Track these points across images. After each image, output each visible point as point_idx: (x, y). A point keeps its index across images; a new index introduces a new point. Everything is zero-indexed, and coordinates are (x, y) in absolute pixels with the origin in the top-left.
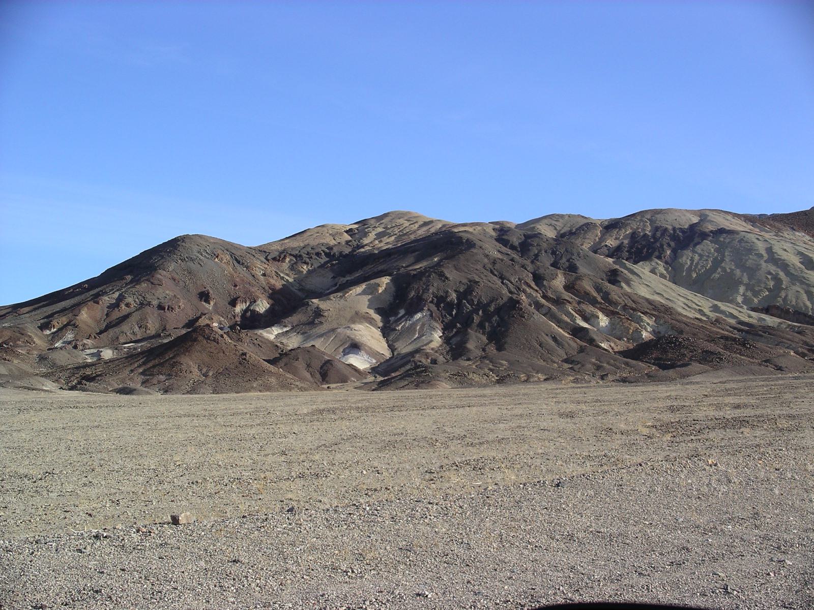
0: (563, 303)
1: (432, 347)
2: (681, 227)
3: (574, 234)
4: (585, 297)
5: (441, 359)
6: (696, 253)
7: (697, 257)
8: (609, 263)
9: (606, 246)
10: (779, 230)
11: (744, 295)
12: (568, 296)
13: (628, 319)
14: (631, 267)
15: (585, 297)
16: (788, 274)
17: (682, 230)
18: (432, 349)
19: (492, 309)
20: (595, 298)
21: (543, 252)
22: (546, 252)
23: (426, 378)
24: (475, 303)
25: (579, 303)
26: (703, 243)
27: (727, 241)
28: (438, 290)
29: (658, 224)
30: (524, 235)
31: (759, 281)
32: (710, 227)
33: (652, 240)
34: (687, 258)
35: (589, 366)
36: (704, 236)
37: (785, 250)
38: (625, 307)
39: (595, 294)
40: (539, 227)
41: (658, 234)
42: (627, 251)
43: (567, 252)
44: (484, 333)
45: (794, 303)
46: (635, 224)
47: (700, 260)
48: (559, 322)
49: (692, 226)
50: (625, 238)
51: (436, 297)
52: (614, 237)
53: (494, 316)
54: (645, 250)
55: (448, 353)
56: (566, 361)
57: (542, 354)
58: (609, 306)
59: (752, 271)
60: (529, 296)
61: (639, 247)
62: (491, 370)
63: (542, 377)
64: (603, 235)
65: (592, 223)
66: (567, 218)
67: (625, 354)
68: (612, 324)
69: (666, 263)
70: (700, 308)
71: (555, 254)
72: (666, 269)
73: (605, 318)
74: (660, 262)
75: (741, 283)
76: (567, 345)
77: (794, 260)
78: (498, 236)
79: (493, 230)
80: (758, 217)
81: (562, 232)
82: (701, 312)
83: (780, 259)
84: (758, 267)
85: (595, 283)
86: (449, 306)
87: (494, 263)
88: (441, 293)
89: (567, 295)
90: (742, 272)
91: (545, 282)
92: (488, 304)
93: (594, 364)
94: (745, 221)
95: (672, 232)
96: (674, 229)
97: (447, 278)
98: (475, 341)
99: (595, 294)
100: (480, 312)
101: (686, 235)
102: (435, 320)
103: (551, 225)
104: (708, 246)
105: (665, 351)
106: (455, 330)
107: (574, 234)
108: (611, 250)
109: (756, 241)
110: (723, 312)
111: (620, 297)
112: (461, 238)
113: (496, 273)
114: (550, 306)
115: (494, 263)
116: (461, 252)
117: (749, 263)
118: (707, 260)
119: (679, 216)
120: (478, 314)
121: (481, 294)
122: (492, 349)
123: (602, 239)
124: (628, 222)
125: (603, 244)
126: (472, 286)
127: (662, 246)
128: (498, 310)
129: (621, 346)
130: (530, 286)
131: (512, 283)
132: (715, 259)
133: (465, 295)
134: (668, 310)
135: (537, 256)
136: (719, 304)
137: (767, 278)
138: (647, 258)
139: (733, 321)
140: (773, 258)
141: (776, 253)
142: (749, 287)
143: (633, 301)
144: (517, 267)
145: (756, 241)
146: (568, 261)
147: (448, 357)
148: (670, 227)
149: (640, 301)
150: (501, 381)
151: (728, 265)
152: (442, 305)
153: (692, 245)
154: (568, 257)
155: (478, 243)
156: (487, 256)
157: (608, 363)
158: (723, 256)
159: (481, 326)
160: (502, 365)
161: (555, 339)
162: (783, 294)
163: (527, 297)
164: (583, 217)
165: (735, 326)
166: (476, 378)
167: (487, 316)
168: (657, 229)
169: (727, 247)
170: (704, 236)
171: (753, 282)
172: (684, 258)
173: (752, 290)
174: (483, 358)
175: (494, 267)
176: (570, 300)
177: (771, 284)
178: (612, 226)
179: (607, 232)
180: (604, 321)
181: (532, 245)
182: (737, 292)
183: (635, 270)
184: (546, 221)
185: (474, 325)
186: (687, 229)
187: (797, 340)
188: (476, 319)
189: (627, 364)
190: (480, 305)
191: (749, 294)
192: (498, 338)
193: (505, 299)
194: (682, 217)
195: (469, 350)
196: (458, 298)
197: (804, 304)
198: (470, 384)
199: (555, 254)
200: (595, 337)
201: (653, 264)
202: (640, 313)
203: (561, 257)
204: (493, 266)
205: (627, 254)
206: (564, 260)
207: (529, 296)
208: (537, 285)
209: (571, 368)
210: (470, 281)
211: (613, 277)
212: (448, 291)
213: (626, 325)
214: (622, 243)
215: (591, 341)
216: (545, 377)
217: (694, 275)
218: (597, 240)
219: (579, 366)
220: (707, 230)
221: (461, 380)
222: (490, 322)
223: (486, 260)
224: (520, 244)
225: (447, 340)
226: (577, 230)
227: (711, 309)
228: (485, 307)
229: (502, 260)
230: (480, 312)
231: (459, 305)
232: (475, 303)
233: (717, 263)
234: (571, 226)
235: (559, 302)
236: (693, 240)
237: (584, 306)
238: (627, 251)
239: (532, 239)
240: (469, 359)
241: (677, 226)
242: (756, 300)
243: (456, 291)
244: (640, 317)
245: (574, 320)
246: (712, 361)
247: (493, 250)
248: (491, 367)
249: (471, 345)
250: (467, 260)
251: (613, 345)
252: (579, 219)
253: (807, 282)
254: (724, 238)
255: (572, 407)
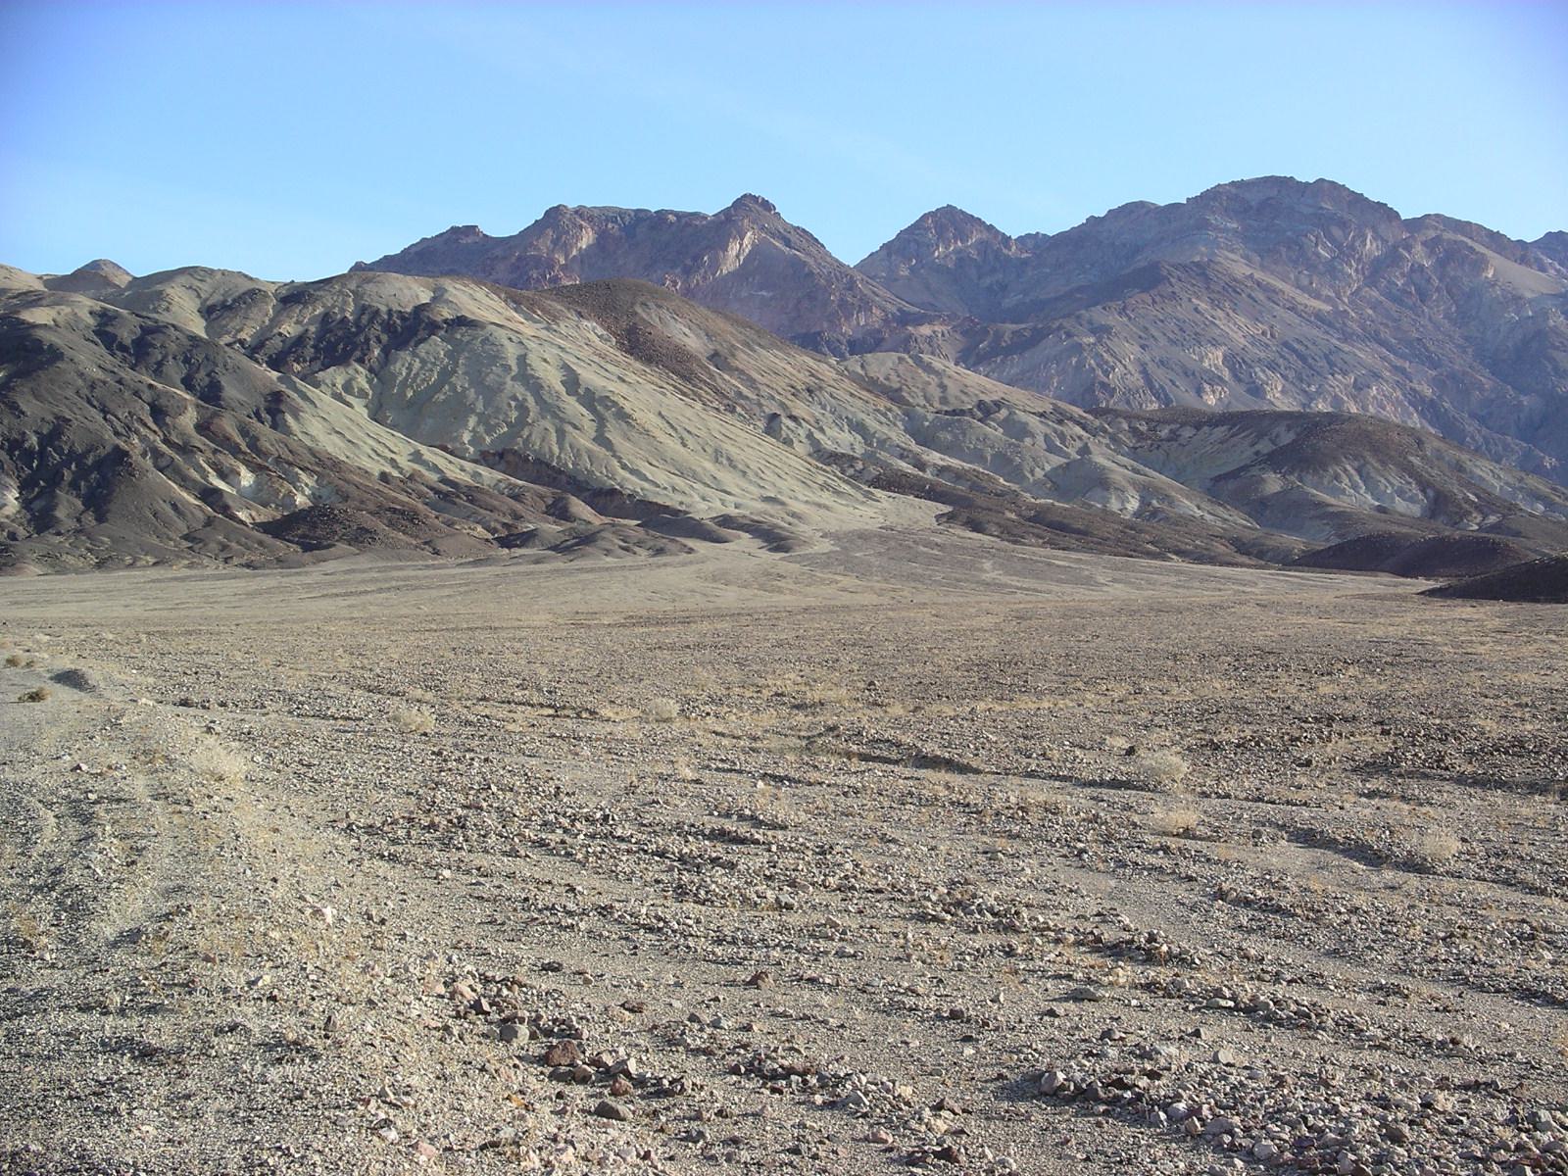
0: (192, 451)
1: (7, 513)
2: (400, 309)
3: (230, 308)
4: (225, 443)
5: (21, 532)
6: (418, 357)
7: (417, 364)
8: (271, 380)
9: (280, 334)
10: (555, 319)
11: (473, 430)
12: (200, 440)
13: (280, 477)
14: (304, 389)
15: (225, 443)
16: (540, 400)
17: (402, 316)
18: (7, 517)
19: (90, 461)
20: (237, 445)
21: (170, 358)
22: (174, 358)
23: (9, 559)
24: (66, 452)
25: (215, 452)
26: (430, 341)
27: (466, 339)
28: (10, 430)
29: (367, 301)
30: (141, 327)
31: (498, 410)
32: (447, 313)
33: (353, 330)
34: (404, 364)
35: (213, 545)
36: (433, 327)
37: (545, 360)
38: (278, 460)
39: (238, 439)
40: (169, 291)
41: (365, 319)
42: (312, 347)
43: (208, 360)
44: (78, 496)
45: (536, 447)
46: (329, 297)
47: (422, 368)
48: (185, 482)
49: (420, 309)
50: (310, 323)
51: (8, 440)
52: (294, 319)
53: (92, 473)
54: (341, 346)
55: (29, 521)
56: (186, 537)
57: (156, 528)
58: (255, 456)
59: (491, 393)
60: (143, 439)
61: (333, 339)
62: (89, 550)
63: (151, 560)
64: (277, 313)
65: (260, 290)
66: (219, 276)
67: (266, 528)
68: (257, 483)
69: (371, 370)
70: (393, 456)
71: (189, 363)
72: (369, 382)
73: (250, 475)
74: (360, 369)
75: (473, 411)
76: (190, 516)
77: (552, 378)
78: (98, 325)
79: (91, 313)
80: (633, 214)
81: (209, 303)
82: (393, 463)
83: (533, 376)
84: (500, 387)
85: (240, 421)
86: (28, 455)
87: (92, 387)
88: (15, 435)
89: (198, 440)
90: (477, 393)
91: (168, 419)
92: (84, 455)
93: (220, 543)
94: (505, 301)
95: (386, 317)
96: (390, 312)
97: (23, 413)
98: (67, 507)
99: (238, 439)
100: (73, 466)
101: (408, 323)
102: (8, 475)
103: (190, 288)
104: (436, 346)
105: (314, 526)
106: (37, 490)
107: (230, 308)
108: (288, 343)
109: (506, 342)
110: (425, 463)
111: (272, 445)
112: (41, 341)
113: (95, 403)
114: (174, 455)
115: (92, 387)
116: (41, 366)
117: (490, 379)
118: (432, 371)
119: (401, 289)
120: (70, 468)
121: (74, 439)
122: (89, 518)
123: (275, 321)
124: (318, 293)
125: (275, 331)
126: (60, 424)
127: (368, 340)
128: (99, 465)
129: (265, 515)
130: (145, 425)
131: (119, 419)
132: (444, 369)
133: (52, 437)
134: (336, 465)
135: (160, 364)
136: (423, 449)
137: (509, 405)
138: (341, 360)
139: (433, 477)
140: (526, 377)
141: (530, 365)
142: (483, 419)
143: (290, 451)
144: (127, 394)
145: (506, 342)
146: (208, 375)
147: (31, 529)
148: (384, 309)
149: (301, 450)
150: (100, 565)
151: (460, 381)
152: (17, 453)
153: (412, 343)
154: (209, 369)
155: (68, 353)
156: (81, 375)
157: (238, 543)
158: (456, 364)
159: (74, 486)
160: (103, 542)
161: (175, 507)
162: (525, 433)
163: (140, 440)
164: (246, 276)
165: (435, 486)
166: (71, 560)
167: (83, 472)
168: (363, 309)
169: (463, 351)
170: (433, 327)
171: (489, 411)
172: (398, 365)
173: (487, 424)
174: (78, 532)
175: (94, 395)
176: (202, 447)
177: (514, 415)
178: (295, 296)
179: (284, 309)
180: (247, 478)
181: (153, 346)
182: (466, 425)
183: (309, 394)
184: (183, 279)
185: (64, 484)
186: (410, 314)
187: (504, 508)
188: (67, 475)
189: (261, 543)
190: (71, 456)
191: (481, 429)
192: (97, 503)
193: (109, 449)
194: (405, 291)
195: (58, 521)
196: (40, 444)
197: (550, 449)
198: (62, 570)
199: (189, 363)
200: (231, 503)
201: (351, 371)
202: (297, 469)
203: (198, 369)
204: (92, 392)
205: (312, 350)
206: (202, 374)
207: (143, 439)
208: (155, 422)
209: (189, 548)
210: (57, 418)
211: (275, 406)
212: (24, 433)
213: (276, 486)
214: (307, 330)
215: (225, 509)
216: (154, 560)
217: (410, 394)
218: (267, 322)
219: (201, 545)
220: (439, 319)
221: (53, 562)
222: (87, 481)
223: (80, 382)
224: (133, 341)
225: (26, 503)
226: (234, 301)
227: (410, 458)
228: (79, 459)
229: (105, 383)
230: (73, 466)
231: (42, 455)
232: (66, 452)
233: (446, 375)
234: (226, 292)
235: (186, 449)
236: (416, 334)
237: (220, 457)
238: (313, 347)
239: (154, 336)
240: (59, 534)
241: (396, 307)
242: (488, 440)
243: (36, 432)
244: (297, 474)
245: (205, 477)
246: (362, 542)
247: (89, 360)
248: (88, 545)
249: (60, 513)
250: (52, 381)
251: (254, 513)
252: (241, 280)
253: (561, 415)
254: (462, 336)
255: (129, 602)
